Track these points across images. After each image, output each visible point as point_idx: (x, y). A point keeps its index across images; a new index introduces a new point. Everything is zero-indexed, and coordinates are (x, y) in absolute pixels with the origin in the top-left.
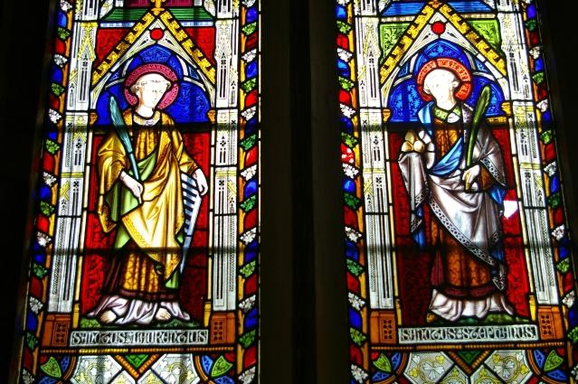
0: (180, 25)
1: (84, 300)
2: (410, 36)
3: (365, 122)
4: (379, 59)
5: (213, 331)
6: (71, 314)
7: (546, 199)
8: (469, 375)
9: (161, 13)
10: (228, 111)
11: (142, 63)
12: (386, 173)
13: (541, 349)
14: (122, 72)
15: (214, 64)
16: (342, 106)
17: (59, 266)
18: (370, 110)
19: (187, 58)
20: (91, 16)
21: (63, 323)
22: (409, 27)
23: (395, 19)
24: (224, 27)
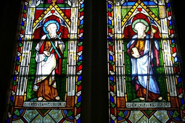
15: (70, 20)
22: (130, 10)
23: (126, 7)
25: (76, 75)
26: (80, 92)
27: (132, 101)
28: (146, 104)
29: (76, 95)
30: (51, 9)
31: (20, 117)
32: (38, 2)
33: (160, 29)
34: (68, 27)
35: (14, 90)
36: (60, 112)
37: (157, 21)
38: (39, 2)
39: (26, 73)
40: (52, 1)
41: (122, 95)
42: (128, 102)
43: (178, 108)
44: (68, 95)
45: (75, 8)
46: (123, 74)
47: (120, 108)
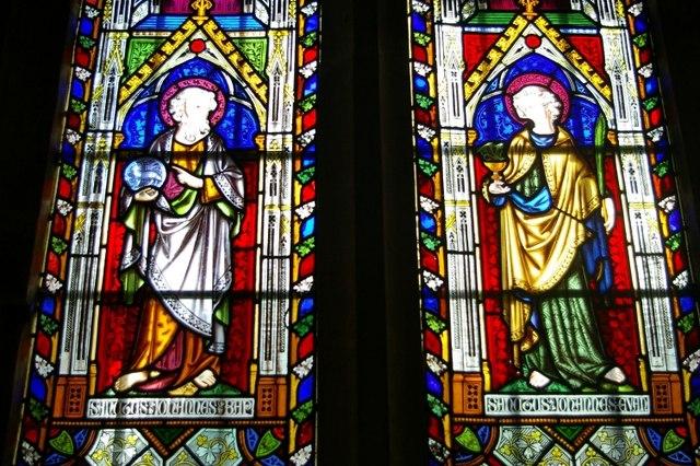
0: (227, 36)
1: (100, 360)
3: (446, 144)
4: (122, 78)
5: (260, 400)
6: (88, 377)
7: (664, 240)
8: (573, 454)
9: (206, 22)
10: (631, 134)
11: (177, 80)
12: (471, 206)
14: (155, 88)
15: (607, 82)
17: (458, 311)
18: (452, 131)
19: (235, 75)
21: (78, 391)
23: (154, 34)
24: (612, 37)
26: (311, 359)
29: (295, 373)
30: (191, 36)
32: (138, 9)
33: (265, 117)
34: (603, 103)
35: (46, 354)
36: (231, 437)
38: (145, 6)
39: (93, 285)
40: (196, 5)
41: (80, 368)
42: (494, 391)
44: (262, 373)
45: (286, 32)
47: (63, 419)
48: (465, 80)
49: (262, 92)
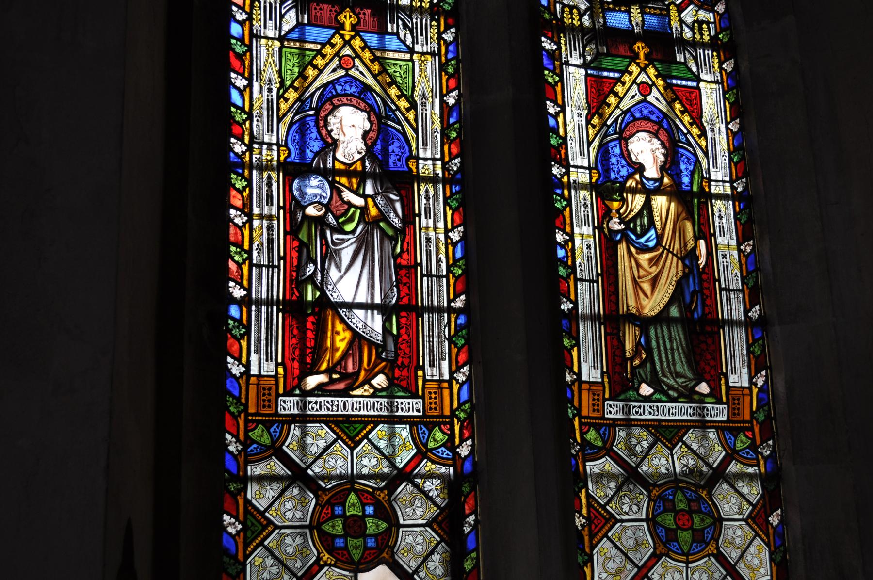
2: (315, 67)
4: (279, 90)
5: (427, 400)
7: (448, 267)
13: (426, 425)
16: (233, 140)
18: (579, 170)
20: (579, 62)
21: (268, 390)
22: (314, 57)
25: (450, 310)
27: (622, 397)
28: (336, 403)
29: (455, 379)
31: (271, 451)
32: (287, 17)
37: (405, 112)
41: (268, 368)
43: (446, 417)
46: (275, 297)
48: (588, 122)
49: (411, 116)
